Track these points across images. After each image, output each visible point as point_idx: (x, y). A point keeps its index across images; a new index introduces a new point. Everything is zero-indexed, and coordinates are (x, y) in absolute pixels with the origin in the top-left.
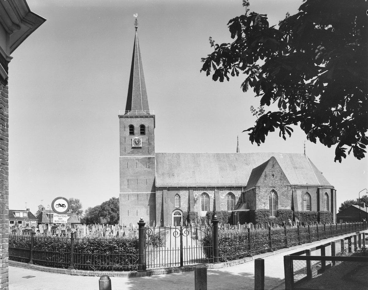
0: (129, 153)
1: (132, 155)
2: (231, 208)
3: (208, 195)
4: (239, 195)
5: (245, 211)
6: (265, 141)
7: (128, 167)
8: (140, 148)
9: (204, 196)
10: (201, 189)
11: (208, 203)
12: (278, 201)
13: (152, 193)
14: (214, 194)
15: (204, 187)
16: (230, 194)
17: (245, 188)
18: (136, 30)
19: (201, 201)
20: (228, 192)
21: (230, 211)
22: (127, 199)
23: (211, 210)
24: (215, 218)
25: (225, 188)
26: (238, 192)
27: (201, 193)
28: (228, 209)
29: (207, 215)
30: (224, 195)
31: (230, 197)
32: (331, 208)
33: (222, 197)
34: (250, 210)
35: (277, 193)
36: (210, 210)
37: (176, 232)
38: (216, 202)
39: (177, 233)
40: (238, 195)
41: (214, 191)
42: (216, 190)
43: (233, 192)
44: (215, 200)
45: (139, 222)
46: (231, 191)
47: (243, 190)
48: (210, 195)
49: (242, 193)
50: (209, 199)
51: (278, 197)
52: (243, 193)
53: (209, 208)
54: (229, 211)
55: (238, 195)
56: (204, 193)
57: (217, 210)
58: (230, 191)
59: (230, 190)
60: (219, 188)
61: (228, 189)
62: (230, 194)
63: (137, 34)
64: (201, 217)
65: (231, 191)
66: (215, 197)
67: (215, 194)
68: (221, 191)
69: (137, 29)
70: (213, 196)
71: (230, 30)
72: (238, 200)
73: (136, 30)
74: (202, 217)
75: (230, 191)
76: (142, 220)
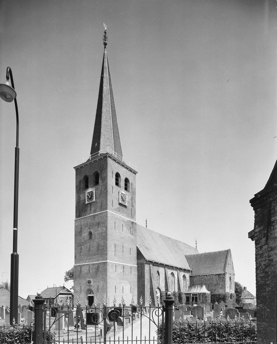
0: (116, 210)
1: (119, 213)
6: (227, 249)
7: (116, 228)
8: (125, 206)
10: (171, 269)
11: (174, 283)
13: (106, 261)
18: (105, 47)
22: (114, 271)
25: (187, 271)
32: (144, 286)
37: (157, 314)
39: (157, 314)
45: (34, 299)
63: (106, 52)
69: (107, 46)
71: (251, 205)
73: (105, 47)
76: (40, 295)
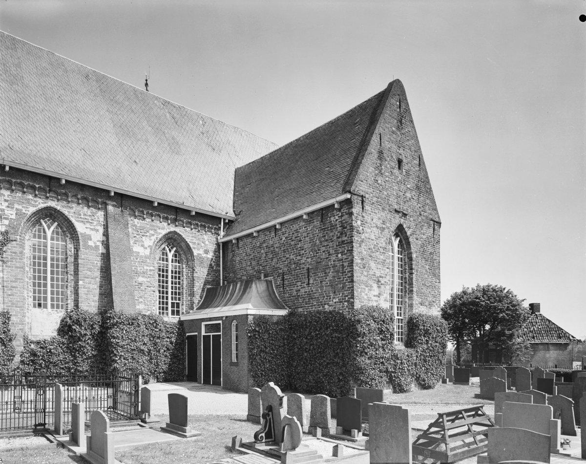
2: (173, 306)
3: (68, 228)
4: (206, 252)
5: (272, 316)
9: (50, 229)
10: (33, 188)
11: (71, 268)
12: (411, 279)
14: (101, 230)
15: (50, 178)
16: (172, 240)
17: (229, 224)
19: (28, 252)
20: (164, 228)
21: (171, 319)
23: (90, 304)
24: (484, 327)
25: (154, 208)
26: (206, 237)
27: (32, 210)
28: (163, 308)
29: (65, 329)
30: (149, 242)
31: (170, 256)
33: (136, 248)
34: (290, 314)
35: (408, 244)
36: (83, 306)
38: (113, 265)
40: (201, 252)
41: (101, 214)
42: (110, 208)
43: (188, 234)
44: (106, 258)
46: (179, 230)
47: (222, 233)
48: (80, 228)
49: (218, 244)
50: (77, 249)
51: (411, 259)
52: (225, 244)
53: (76, 293)
54: (166, 319)
55: (201, 252)
56: (50, 214)
57: (122, 305)
58: (172, 228)
59: (174, 221)
60: (125, 203)
61: (166, 219)
62: (172, 240)
64: (27, 342)
65: (179, 230)
66: (106, 245)
67: (106, 227)
68: (136, 220)
70: (97, 237)
72: (205, 271)
74: (38, 343)
75: (172, 228)
